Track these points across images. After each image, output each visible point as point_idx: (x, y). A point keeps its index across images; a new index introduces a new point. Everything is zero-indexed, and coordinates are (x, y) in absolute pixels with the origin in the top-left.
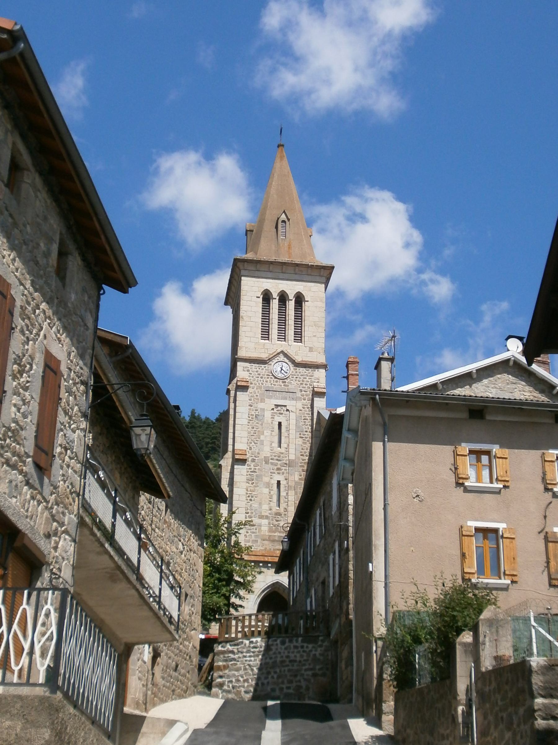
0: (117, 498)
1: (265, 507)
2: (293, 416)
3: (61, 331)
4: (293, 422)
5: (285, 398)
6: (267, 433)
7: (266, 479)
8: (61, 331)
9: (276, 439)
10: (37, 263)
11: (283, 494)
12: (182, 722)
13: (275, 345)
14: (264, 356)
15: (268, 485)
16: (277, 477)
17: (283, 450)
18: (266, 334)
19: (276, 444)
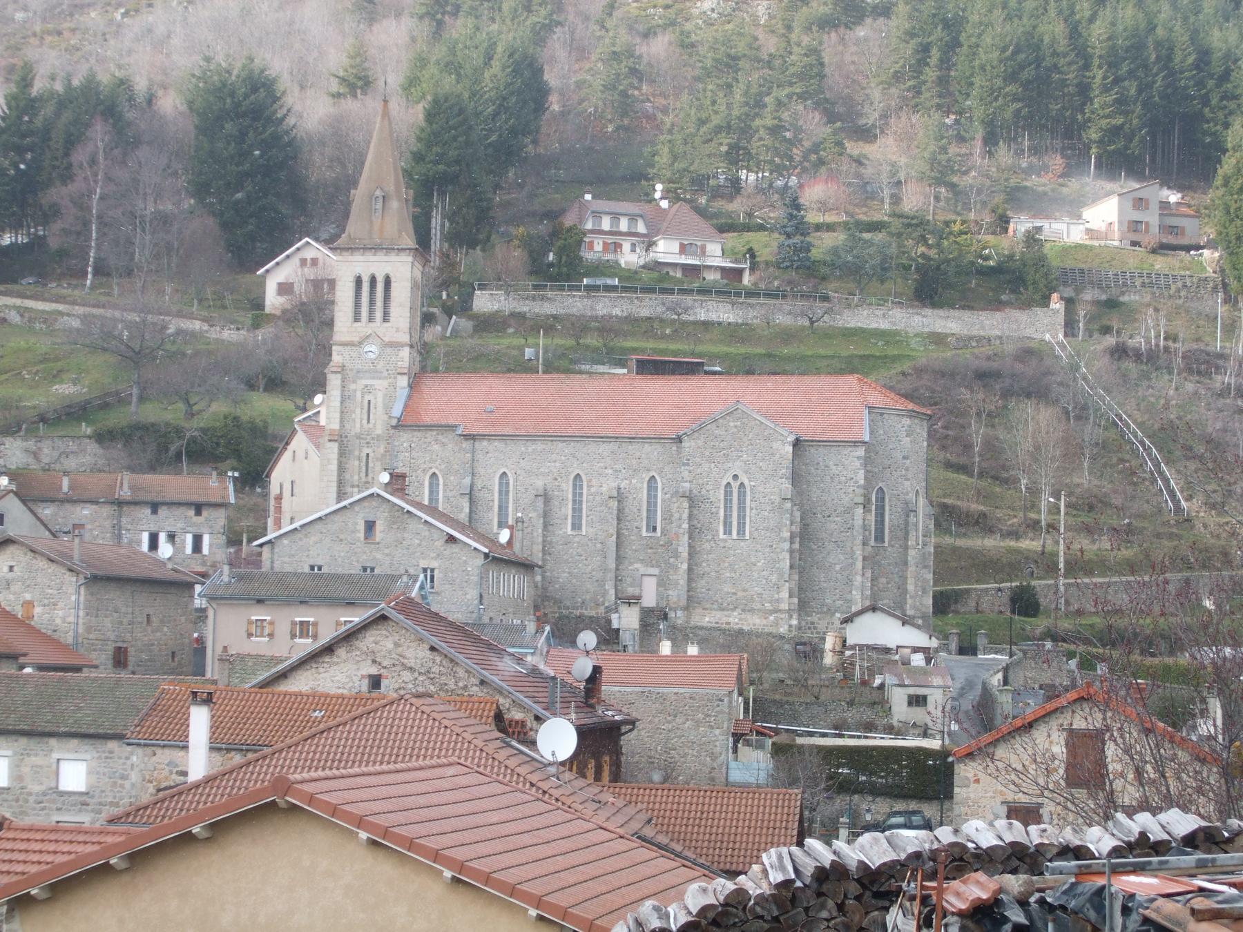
0: (876, 913)
1: (356, 477)
2: (380, 395)
3: (1175, 488)
4: (380, 399)
5: (373, 378)
6: (358, 411)
7: (357, 453)
8: (1175, 488)
9: (365, 417)
10: (119, 86)
11: (371, 465)
12: (22, 544)
13: (363, 328)
14: (356, 339)
15: (359, 459)
16: (366, 451)
17: (371, 425)
18: (357, 319)
19: (365, 421)
